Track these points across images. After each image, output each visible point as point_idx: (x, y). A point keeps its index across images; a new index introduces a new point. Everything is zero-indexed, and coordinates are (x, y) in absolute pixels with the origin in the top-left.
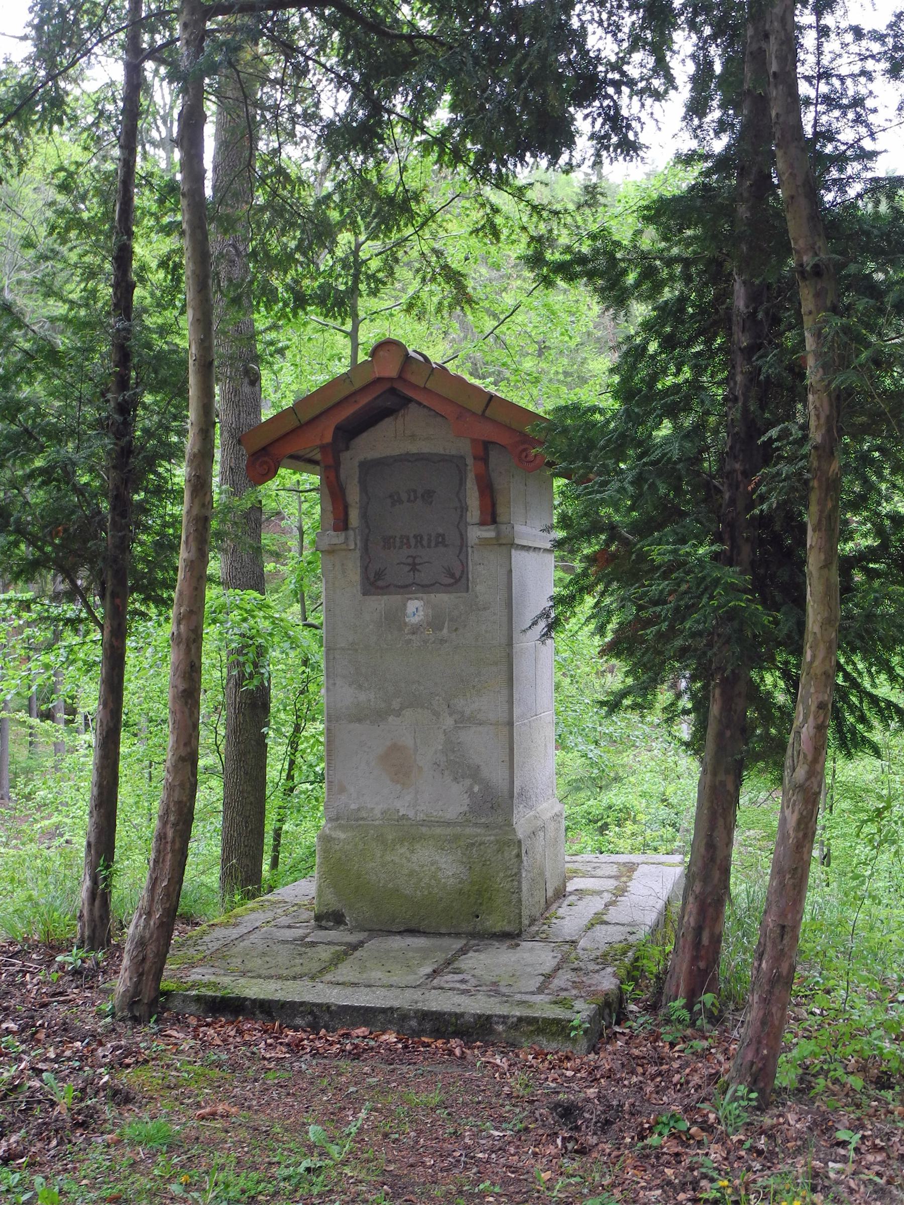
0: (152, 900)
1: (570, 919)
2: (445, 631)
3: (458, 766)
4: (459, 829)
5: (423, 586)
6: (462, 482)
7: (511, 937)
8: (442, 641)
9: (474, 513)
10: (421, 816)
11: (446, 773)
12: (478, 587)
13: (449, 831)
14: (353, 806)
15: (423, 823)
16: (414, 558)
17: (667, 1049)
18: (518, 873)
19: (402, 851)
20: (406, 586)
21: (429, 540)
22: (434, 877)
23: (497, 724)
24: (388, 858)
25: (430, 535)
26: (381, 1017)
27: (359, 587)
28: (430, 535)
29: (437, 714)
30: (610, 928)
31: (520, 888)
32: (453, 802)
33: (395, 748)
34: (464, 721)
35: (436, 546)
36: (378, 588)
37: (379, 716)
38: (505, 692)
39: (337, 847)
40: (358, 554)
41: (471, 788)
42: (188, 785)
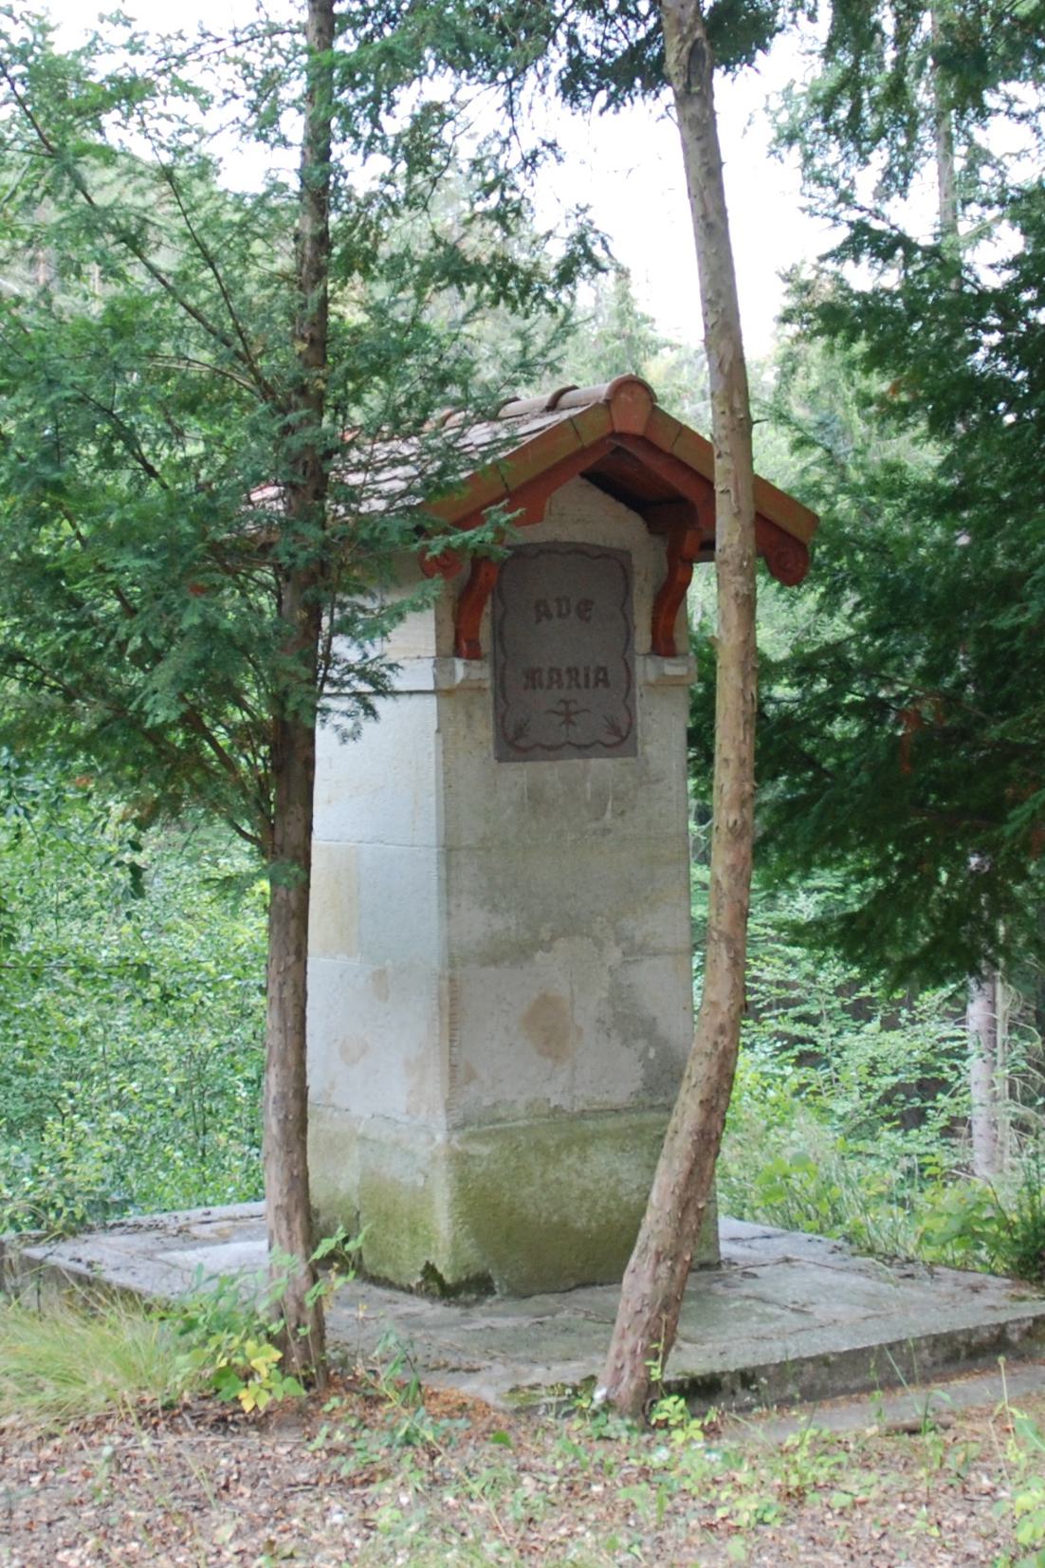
4: (635, 1119)
5: (579, 747)
8: (606, 831)
9: (643, 639)
10: (581, 1105)
11: (613, 1033)
12: (648, 748)
13: (622, 1122)
14: (487, 1102)
19: (569, 1162)
21: (587, 676)
24: (551, 1176)
25: (587, 669)
27: (491, 747)
28: (587, 669)
29: (599, 944)
30: (130, 1332)
33: (546, 1002)
34: (636, 952)
39: (479, 1170)
40: (489, 697)
41: (646, 1050)
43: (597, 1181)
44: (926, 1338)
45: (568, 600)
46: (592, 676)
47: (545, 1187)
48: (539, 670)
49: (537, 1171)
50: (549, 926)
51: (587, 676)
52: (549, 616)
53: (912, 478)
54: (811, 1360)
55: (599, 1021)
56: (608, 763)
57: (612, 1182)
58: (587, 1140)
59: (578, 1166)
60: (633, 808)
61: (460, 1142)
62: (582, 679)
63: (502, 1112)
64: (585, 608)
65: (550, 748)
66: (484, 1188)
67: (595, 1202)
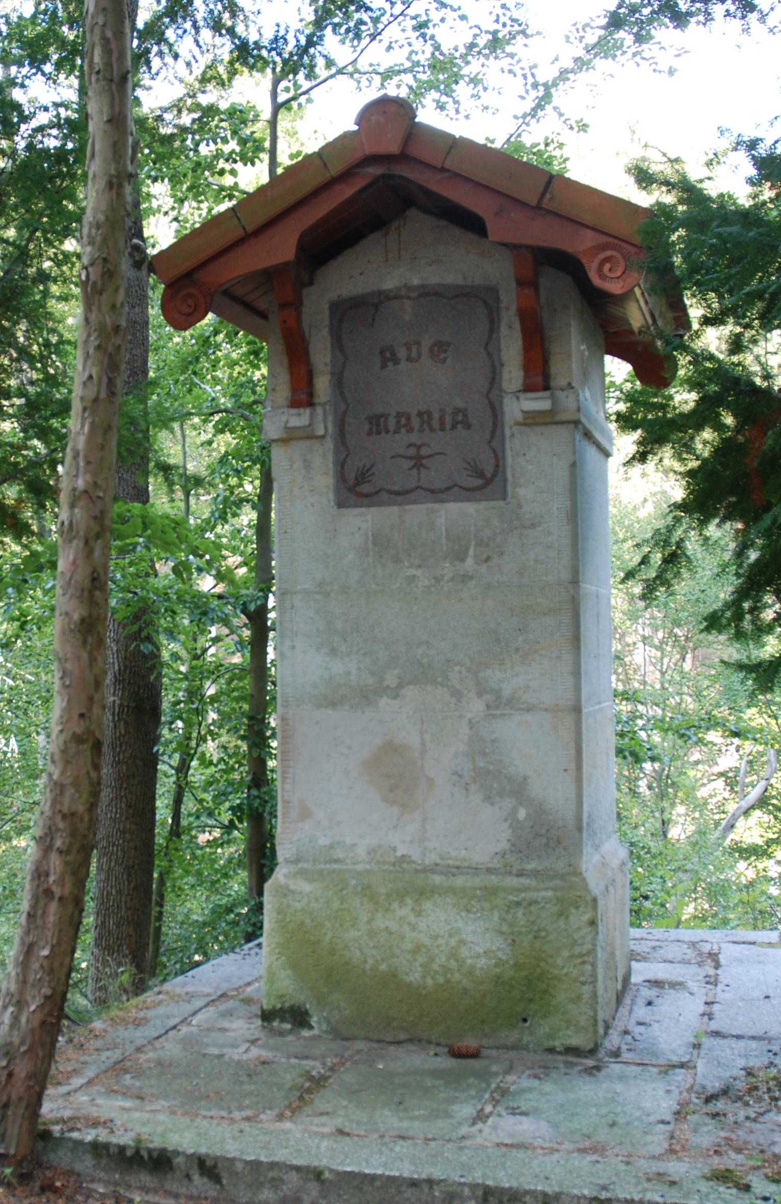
0: (23, 982)
1: (671, 1024)
2: (470, 561)
3: (491, 777)
4: (494, 880)
5: (433, 491)
6: (493, 326)
7: (586, 1056)
8: (465, 578)
9: (513, 374)
12: (521, 492)
13: (477, 881)
14: (323, 841)
15: (433, 869)
16: (419, 447)
18: (592, 951)
22: (454, 955)
23: (554, 710)
24: (380, 923)
25: (442, 411)
26: (409, 1193)
28: (442, 411)
31: (594, 975)
32: (474, 833)
34: (500, 705)
35: (454, 427)
36: (494, 475)
37: (367, 697)
38: (568, 657)
39: (298, 906)
40: (329, 444)
41: (514, 812)
42: (86, 787)
43: (436, 937)
44: (474, 1187)
45: (418, 344)
46: (448, 420)
47: (372, 934)
48: (386, 416)
49: (364, 917)
50: (396, 672)
52: (396, 361)
54: (298, 1169)
55: (455, 773)
56: (470, 507)
57: (453, 942)
58: (424, 893)
59: (412, 918)
60: (502, 554)
61: (286, 876)
62: (435, 423)
63: (339, 854)
65: (398, 493)
66: (303, 923)
67: (432, 959)
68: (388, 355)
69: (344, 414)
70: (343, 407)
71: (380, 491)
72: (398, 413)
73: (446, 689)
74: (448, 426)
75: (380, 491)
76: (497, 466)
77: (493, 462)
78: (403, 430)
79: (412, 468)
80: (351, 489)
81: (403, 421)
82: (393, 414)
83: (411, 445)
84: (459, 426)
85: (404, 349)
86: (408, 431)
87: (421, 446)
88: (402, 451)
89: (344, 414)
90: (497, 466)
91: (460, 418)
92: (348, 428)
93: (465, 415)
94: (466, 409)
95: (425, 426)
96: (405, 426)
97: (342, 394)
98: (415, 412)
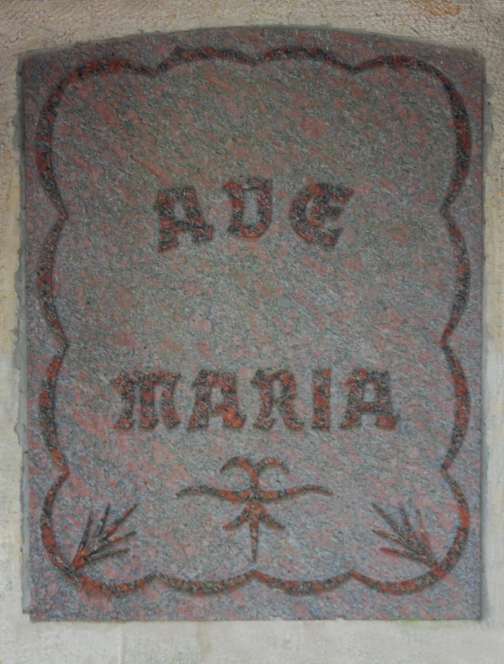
5: (291, 588)
16: (258, 469)
17: (106, 468)
20: (225, 587)
21: (321, 394)
25: (323, 374)
28: (323, 374)
35: (351, 421)
36: (455, 553)
45: (264, 187)
46: (338, 401)
48: (173, 381)
51: (321, 394)
52: (202, 232)
53: (190, 232)
62: (304, 406)
64: (320, 207)
68: (179, 212)
69: (56, 366)
70: (51, 348)
71: (149, 579)
72: (203, 374)
73: (154, 66)
74: (336, 417)
75: (149, 579)
76: (463, 530)
77: (453, 518)
78: (216, 421)
79: (240, 521)
80: (72, 571)
81: (217, 396)
82: (190, 375)
83: (234, 462)
84: (366, 419)
85: (223, 199)
86: (227, 424)
87: (262, 467)
88: (210, 476)
89: (56, 366)
90: (463, 530)
91: (369, 397)
92: (64, 408)
93: (383, 391)
94: (385, 374)
95: (276, 413)
96: (222, 408)
97: (49, 309)
98: (250, 374)
